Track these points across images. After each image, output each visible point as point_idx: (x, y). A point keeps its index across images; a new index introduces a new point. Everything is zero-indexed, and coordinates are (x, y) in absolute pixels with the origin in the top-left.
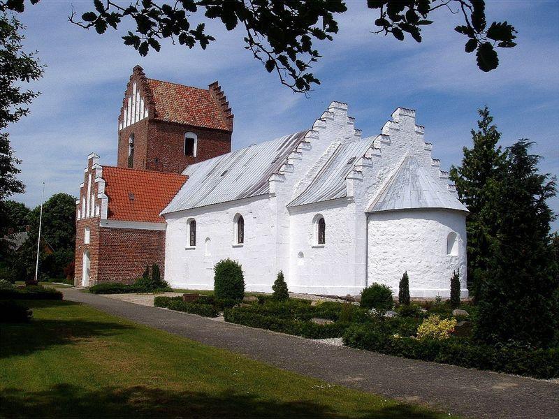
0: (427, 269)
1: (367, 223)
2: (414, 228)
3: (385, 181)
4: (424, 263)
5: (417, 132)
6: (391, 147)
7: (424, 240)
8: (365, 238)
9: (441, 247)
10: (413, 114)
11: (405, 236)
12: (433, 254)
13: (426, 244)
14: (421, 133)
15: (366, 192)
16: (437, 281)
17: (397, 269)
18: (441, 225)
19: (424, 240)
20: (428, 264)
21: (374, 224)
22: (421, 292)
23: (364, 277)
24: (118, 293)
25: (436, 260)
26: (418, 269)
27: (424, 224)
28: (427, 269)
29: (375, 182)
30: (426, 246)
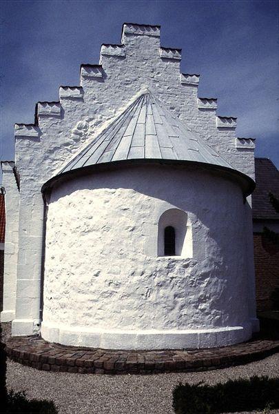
0: (111, 288)
1: (46, 209)
2: (90, 208)
3: (91, 137)
4: (104, 276)
5: (165, 59)
6: (107, 83)
7: (106, 228)
8: (39, 236)
9: (143, 241)
10: (158, 32)
11: (74, 225)
12: (122, 256)
13: (110, 236)
14: (172, 60)
15: (46, 158)
16: (132, 313)
17: (62, 290)
18: (142, 198)
19: (106, 228)
20: (110, 277)
21: (60, 208)
22: (96, 338)
23: (37, 302)
24: (190, 334)
25: (129, 269)
26: (92, 288)
27: (106, 197)
28: (111, 288)
29: (68, 140)
30: (109, 241)
